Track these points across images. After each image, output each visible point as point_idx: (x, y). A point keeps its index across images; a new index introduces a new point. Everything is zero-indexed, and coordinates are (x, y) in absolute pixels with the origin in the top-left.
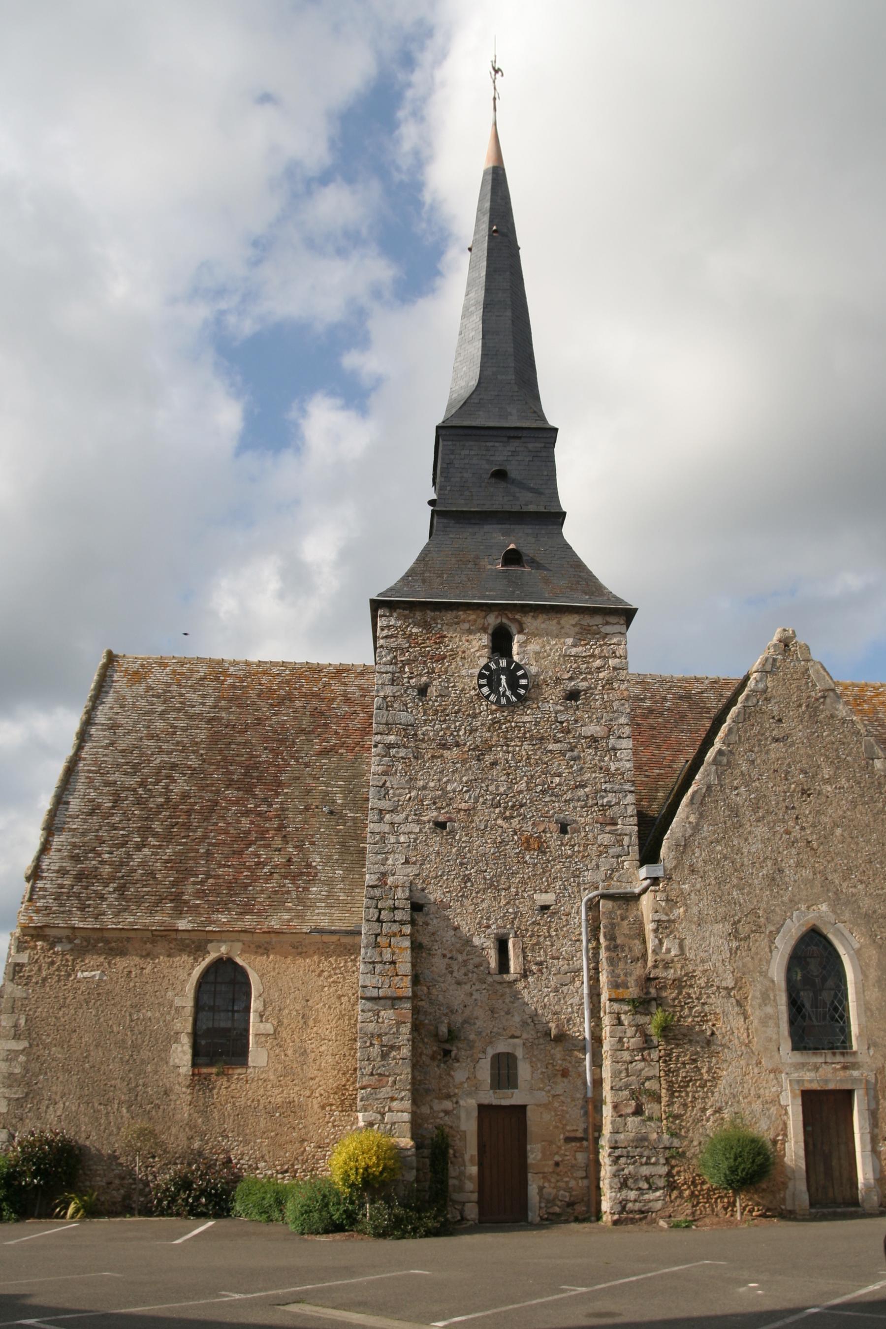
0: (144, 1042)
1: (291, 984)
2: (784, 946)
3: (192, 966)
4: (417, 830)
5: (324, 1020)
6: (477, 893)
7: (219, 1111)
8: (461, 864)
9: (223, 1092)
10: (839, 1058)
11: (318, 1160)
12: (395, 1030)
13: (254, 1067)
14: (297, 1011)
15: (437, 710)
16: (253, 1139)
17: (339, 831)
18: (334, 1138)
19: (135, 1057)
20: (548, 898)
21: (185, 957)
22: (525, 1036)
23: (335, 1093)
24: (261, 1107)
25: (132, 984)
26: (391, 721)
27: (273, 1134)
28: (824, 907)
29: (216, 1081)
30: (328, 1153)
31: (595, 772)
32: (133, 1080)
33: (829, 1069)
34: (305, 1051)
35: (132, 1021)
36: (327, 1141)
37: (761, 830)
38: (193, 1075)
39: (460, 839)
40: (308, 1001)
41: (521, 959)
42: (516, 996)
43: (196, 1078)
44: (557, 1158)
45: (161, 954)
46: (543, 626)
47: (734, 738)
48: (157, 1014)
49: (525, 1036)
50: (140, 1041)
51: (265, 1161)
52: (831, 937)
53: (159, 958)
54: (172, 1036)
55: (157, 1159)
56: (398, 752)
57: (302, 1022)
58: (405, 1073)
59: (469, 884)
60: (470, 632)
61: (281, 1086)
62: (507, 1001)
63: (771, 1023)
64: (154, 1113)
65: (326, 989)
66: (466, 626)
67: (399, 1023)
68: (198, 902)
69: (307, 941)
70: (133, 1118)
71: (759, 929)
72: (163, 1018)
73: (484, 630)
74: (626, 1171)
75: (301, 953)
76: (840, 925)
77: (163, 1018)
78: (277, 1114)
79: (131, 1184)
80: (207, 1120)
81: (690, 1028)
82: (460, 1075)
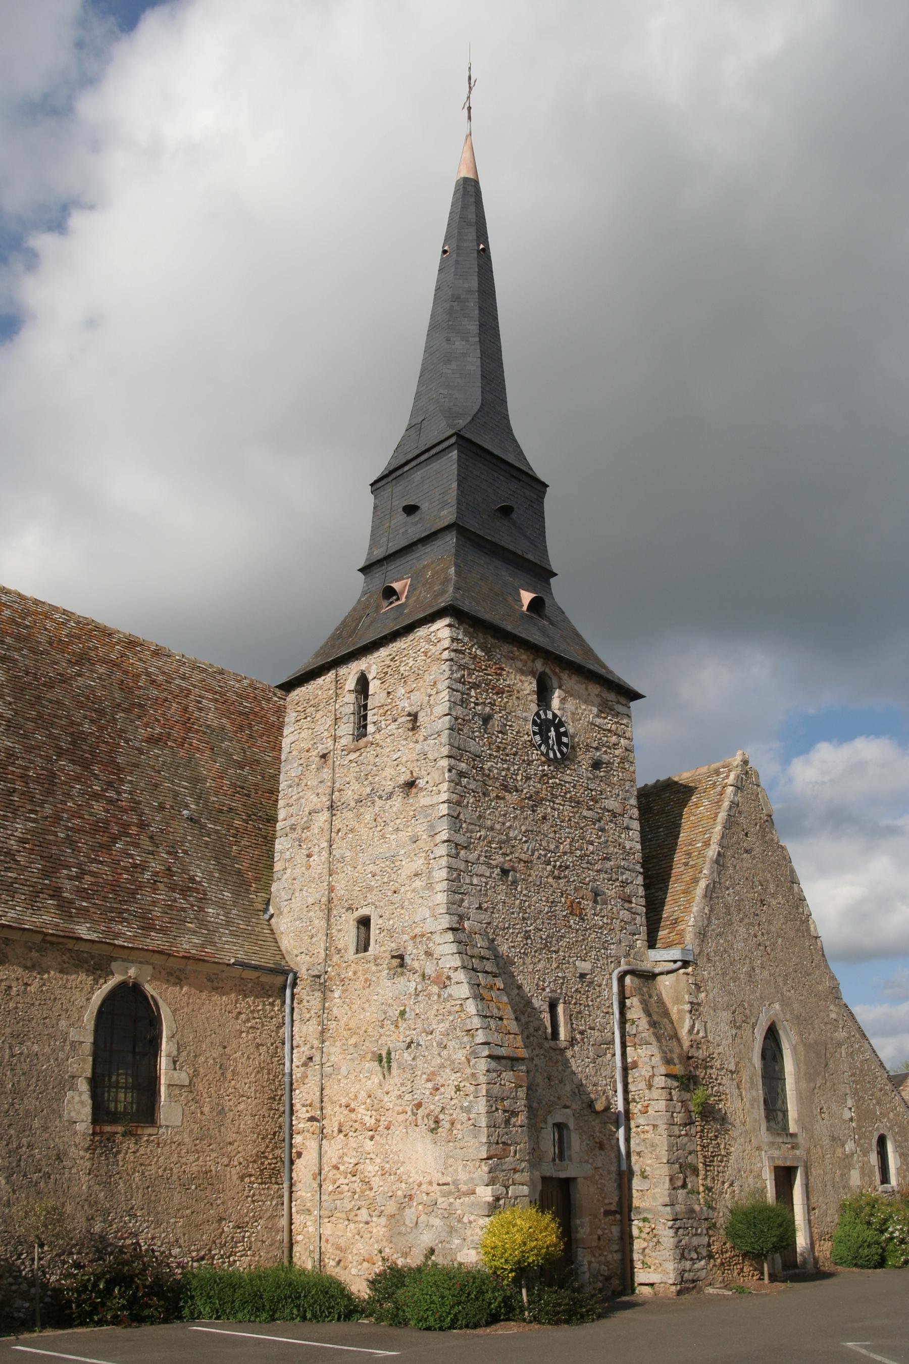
0: (29, 1086)
1: (206, 1025)
3: (92, 988)
4: (488, 874)
5: (243, 1072)
6: (535, 952)
7: (125, 1183)
8: (524, 919)
9: (130, 1157)
11: (236, 1243)
12: (514, 1094)
13: (167, 1126)
14: (214, 1059)
15: (499, 747)
16: (166, 1218)
17: (207, 843)
18: (254, 1216)
19: (17, 1107)
21: (82, 976)
22: (574, 1106)
23: (255, 1162)
24: (175, 1177)
25: (12, 1005)
26: (462, 747)
27: (188, 1212)
29: (121, 1143)
30: (247, 1234)
31: (615, 847)
32: (14, 1138)
34: (223, 1108)
35: (13, 1056)
36: (246, 1219)
38: (94, 1134)
39: (521, 892)
40: (225, 1047)
41: (569, 1026)
43: (97, 1138)
44: (600, 1232)
45: (51, 967)
46: (576, 687)
48: (47, 1049)
49: (574, 1106)
50: (23, 1085)
51: (180, 1247)
52: (781, 1032)
53: (49, 973)
54: (66, 1081)
55: (46, 1248)
56: (468, 783)
57: (219, 1073)
59: (529, 941)
60: (522, 672)
61: (197, 1151)
62: (560, 1068)
64: (42, 1185)
65: (244, 1035)
66: (519, 664)
67: (518, 1086)
68: (84, 904)
69: (224, 974)
70: (14, 1191)
72: (55, 1055)
73: (532, 673)
74: (683, 1243)
75: (217, 988)
77: (55, 1055)
78: (193, 1187)
79: (11, 1284)
80: (111, 1194)
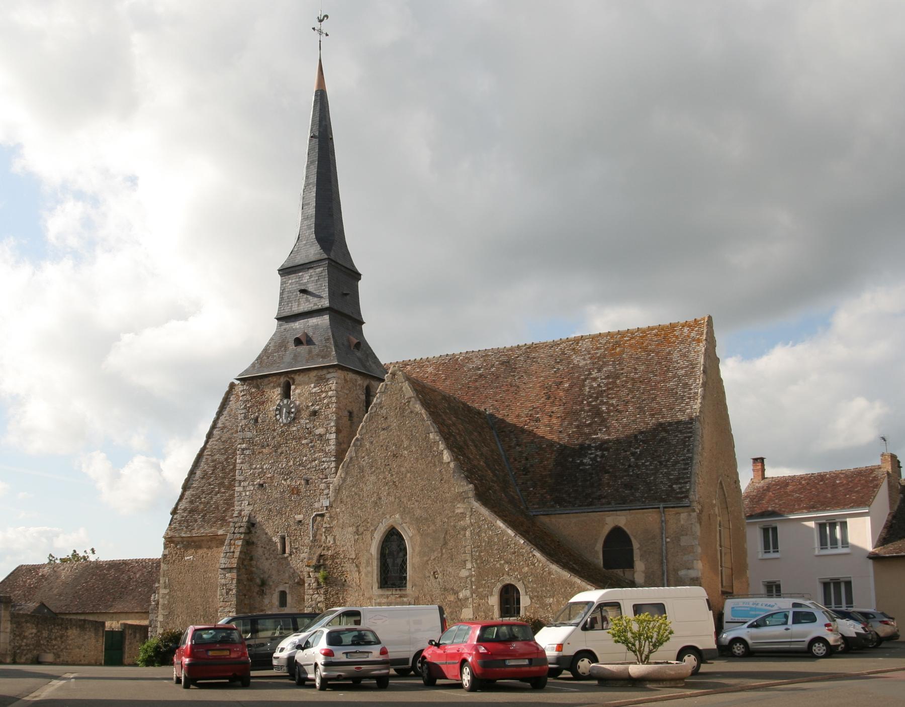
2: (378, 536)
10: (398, 592)
20: (299, 517)
28: (397, 516)
33: (393, 597)
37: (373, 478)
42: (288, 564)
47: (364, 431)
58: (234, 601)
63: (370, 575)
71: (367, 530)
73: (279, 385)
76: (404, 525)
81: (336, 578)
82: (266, 601)
